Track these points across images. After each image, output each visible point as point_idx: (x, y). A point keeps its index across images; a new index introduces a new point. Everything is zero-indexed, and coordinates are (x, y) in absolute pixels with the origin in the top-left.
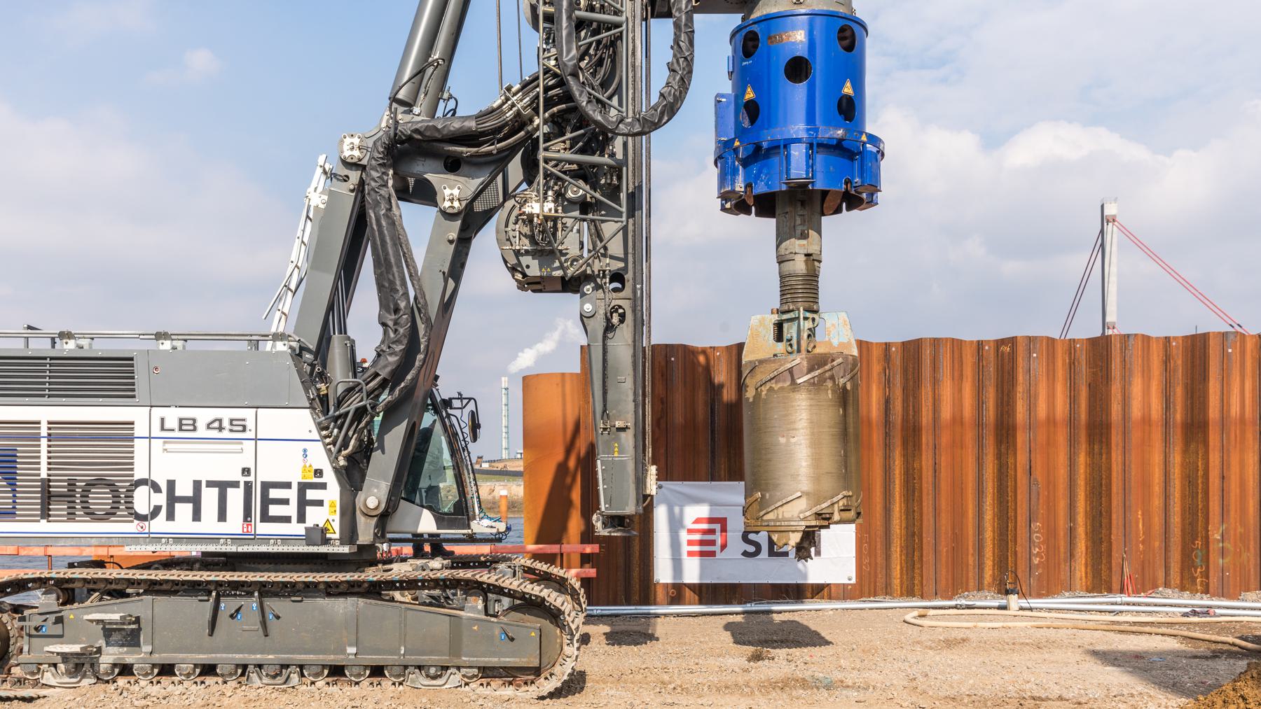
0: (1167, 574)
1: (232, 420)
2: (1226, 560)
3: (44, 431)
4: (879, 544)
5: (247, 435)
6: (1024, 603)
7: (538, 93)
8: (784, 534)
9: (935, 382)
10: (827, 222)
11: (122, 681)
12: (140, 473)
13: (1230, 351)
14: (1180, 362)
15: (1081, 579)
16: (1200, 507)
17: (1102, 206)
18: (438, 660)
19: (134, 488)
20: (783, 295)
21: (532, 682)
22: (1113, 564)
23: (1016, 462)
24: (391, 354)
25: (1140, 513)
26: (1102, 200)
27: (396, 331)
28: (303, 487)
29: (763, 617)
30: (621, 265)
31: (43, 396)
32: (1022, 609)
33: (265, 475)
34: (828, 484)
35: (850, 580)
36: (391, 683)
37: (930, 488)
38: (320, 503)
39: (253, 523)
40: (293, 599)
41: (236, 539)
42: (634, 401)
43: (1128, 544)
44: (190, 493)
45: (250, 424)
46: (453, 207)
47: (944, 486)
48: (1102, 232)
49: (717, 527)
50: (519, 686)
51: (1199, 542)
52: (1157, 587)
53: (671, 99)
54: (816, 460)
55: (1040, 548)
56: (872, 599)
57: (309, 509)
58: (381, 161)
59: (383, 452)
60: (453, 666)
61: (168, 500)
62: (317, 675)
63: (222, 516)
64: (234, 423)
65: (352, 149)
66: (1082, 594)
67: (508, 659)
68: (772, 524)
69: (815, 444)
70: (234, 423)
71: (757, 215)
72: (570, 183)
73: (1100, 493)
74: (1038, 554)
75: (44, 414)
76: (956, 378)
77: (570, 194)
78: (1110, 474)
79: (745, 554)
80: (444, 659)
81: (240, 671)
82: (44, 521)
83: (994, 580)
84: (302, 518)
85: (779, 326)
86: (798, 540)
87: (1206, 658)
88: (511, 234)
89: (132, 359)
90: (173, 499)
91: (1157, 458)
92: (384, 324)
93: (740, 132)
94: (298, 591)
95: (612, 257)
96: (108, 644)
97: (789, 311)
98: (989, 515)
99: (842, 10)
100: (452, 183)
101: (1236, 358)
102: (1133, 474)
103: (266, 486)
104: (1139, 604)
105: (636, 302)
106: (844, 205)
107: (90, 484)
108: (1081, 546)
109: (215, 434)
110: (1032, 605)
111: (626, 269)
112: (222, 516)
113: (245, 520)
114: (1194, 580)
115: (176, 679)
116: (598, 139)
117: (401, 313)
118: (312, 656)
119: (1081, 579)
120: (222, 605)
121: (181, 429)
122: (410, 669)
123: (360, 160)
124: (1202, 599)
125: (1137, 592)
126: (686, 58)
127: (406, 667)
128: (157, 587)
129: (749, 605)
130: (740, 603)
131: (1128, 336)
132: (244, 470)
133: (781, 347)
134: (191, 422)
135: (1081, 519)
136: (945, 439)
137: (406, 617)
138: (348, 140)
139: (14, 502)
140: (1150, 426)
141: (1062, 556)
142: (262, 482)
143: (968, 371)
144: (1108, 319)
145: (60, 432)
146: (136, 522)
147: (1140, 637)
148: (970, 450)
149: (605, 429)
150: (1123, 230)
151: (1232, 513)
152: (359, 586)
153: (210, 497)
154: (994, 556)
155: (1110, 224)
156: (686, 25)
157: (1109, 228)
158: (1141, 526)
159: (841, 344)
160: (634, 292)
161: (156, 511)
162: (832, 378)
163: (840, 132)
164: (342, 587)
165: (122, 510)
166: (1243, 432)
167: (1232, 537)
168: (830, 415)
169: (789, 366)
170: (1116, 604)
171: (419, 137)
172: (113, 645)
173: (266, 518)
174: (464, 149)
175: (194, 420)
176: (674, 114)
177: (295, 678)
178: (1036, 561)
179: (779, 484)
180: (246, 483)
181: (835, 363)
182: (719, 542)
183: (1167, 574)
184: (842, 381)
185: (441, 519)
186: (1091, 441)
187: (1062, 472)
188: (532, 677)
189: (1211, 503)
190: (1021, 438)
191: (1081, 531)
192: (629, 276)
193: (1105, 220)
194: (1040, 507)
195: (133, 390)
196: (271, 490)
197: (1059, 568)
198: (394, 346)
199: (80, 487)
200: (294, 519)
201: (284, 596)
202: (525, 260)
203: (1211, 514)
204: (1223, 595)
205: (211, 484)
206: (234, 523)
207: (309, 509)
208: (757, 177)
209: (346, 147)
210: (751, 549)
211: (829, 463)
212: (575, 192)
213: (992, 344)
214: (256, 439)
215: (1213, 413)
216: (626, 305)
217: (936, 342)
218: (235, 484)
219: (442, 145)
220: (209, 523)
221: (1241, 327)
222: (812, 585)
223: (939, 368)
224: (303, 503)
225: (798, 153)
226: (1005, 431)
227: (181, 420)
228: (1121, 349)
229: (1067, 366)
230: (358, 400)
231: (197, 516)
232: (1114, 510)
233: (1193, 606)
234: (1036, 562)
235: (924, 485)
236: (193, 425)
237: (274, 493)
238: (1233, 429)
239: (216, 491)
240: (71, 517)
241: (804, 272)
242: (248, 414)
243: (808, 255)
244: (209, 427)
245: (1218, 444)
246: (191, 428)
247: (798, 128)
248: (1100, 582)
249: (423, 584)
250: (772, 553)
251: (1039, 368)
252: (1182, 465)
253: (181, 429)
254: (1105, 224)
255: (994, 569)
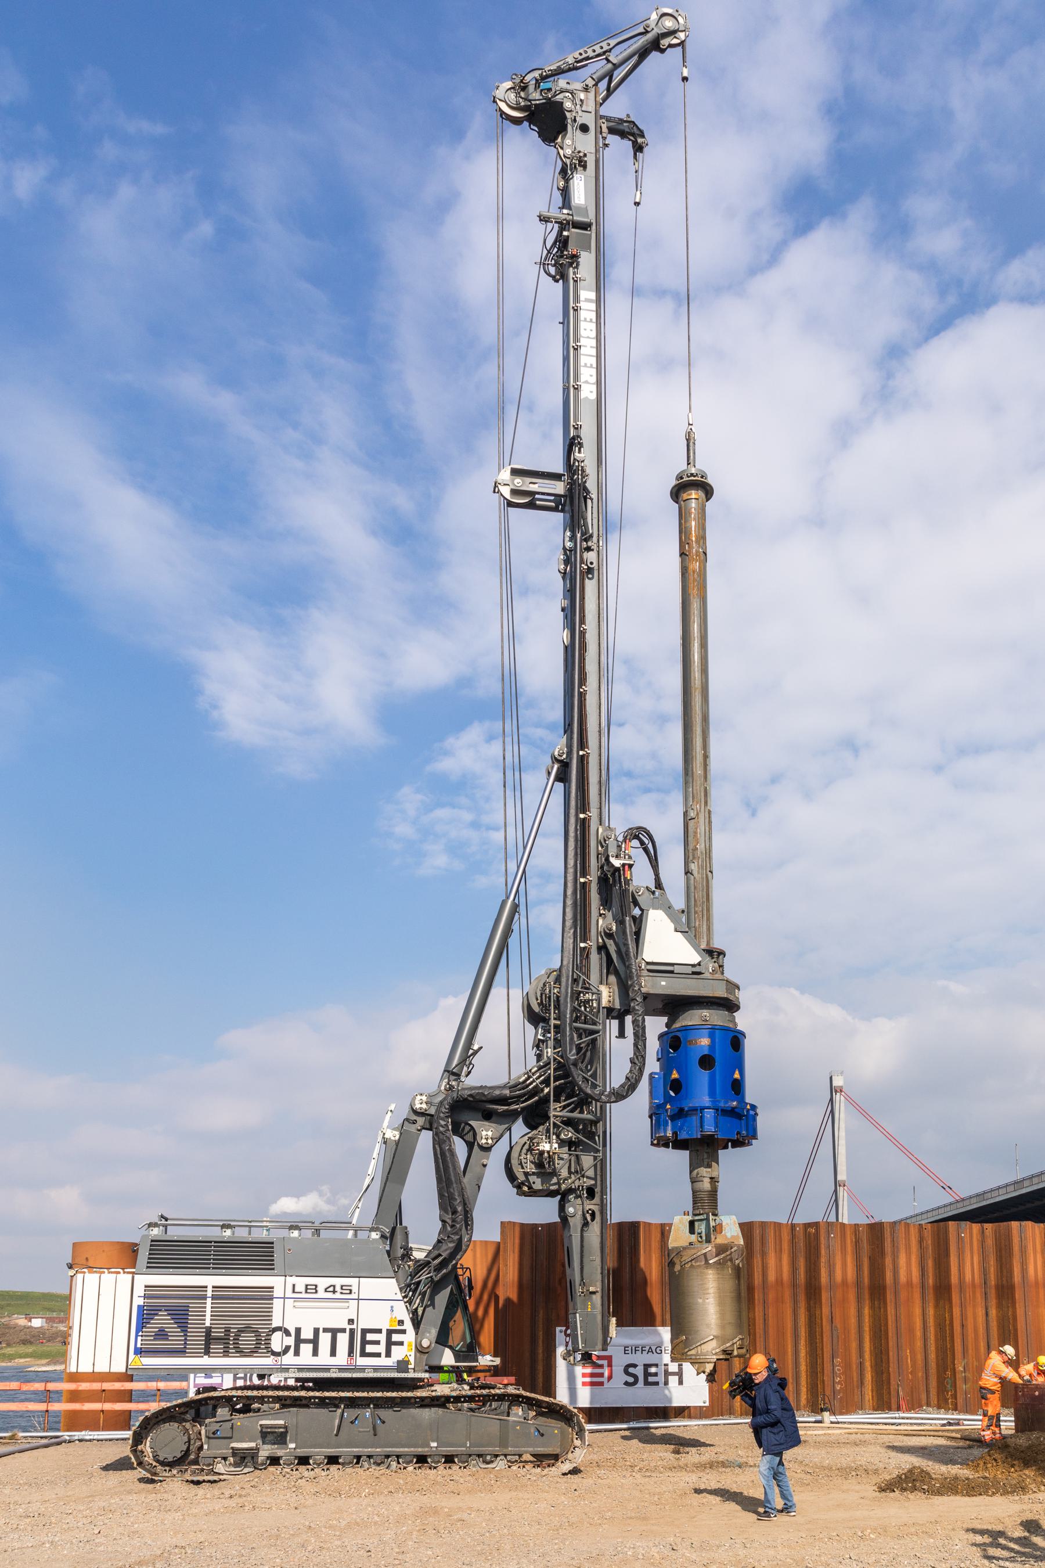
0: (928, 1397)
1: (342, 1286)
2: (968, 1386)
3: (209, 1293)
4: (724, 1375)
5: (354, 1296)
6: (833, 1418)
7: (550, 1074)
8: (702, 1364)
9: (764, 1254)
10: (721, 1153)
11: (271, 1469)
12: (276, 1322)
13: (963, 1235)
14: (930, 1242)
15: (869, 1401)
16: (948, 1347)
17: (831, 1078)
18: (493, 1450)
19: (271, 1333)
20: (696, 1203)
21: (553, 1465)
22: (892, 1390)
23: (822, 1314)
24: (450, 1242)
25: (908, 1351)
26: (830, 1073)
27: (452, 1226)
28: (390, 1333)
29: (646, 1432)
30: (593, 1182)
31: (209, 1268)
32: (832, 1423)
33: (363, 1324)
34: (730, 1330)
35: (704, 1403)
36: (458, 1467)
37: (762, 1333)
38: (401, 1343)
39: (354, 1357)
40: (395, 1409)
41: (341, 1370)
42: (602, 1273)
43: (901, 1374)
44: (311, 1336)
45: (355, 1289)
46: (488, 1143)
47: (772, 1331)
48: (831, 1100)
49: (605, 1362)
50: (545, 1468)
51: (949, 1373)
52: (922, 1406)
53: (633, 1081)
54: (722, 1314)
55: (840, 1378)
56: (721, 1417)
57: (393, 1348)
58: (447, 1115)
59: (434, 1308)
60: (502, 1454)
61: (295, 1341)
62: (409, 1463)
63: (333, 1353)
64: (344, 1288)
65: (421, 1103)
66: (870, 1412)
67: (539, 1449)
68: (694, 1357)
69: (721, 1303)
70: (344, 1288)
71: (673, 1148)
72: (563, 1128)
73: (880, 1337)
74: (839, 1383)
75: (210, 1281)
76: (778, 1250)
77: (562, 1136)
78: (887, 1322)
79: (626, 1383)
80: (497, 1450)
81: (355, 1461)
82: (206, 1357)
83: (808, 1402)
84: (388, 1354)
85: (692, 1224)
86: (711, 1368)
87: (965, 1448)
88: (523, 1161)
89: (272, 1243)
90: (299, 1341)
91: (917, 1311)
92: (443, 1221)
93: (668, 1099)
94: (397, 1404)
95: (588, 1177)
96: (264, 1443)
97: (700, 1214)
98: (803, 1353)
99: (731, 1026)
100: (488, 1127)
101: (967, 1240)
102: (902, 1322)
103: (365, 1332)
104: (911, 1418)
105: (603, 1206)
106: (730, 1144)
107: (241, 1331)
108: (868, 1376)
109: (330, 1295)
110: (839, 1420)
111: (595, 1185)
112: (333, 1353)
113: (349, 1355)
114: (946, 1400)
115: (310, 1467)
116: (584, 1102)
117: (458, 1214)
118: (406, 1449)
119: (869, 1401)
120: (345, 1414)
121: (306, 1292)
122: (474, 1457)
123: (426, 1111)
124: (953, 1414)
125: (909, 1410)
126: (642, 1056)
127: (470, 1455)
128: (298, 1402)
129: (631, 1423)
130: (622, 1422)
131: (895, 1223)
132: (349, 1320)
133: (693, 1238)
134: (314, 1287)
135: (867, 1356)
136: (771, 1296)
137: (470, 1421)
138: (419, 1097)
139: (185, 1343)
140: (912, 1288)
141: (855, 1383)
142: (362, 1329)
143: (786, 1246)
144: (839, 1178)
145: (221, 1294)
146: (272, 1357)
147: (920, 1437)
148: (788, 1305)
149: (582, 1293)
150: (849, 1100)
151: (970, 1351)
152: (437, 1400)
153: (325, 1339)
154: (807, 1385)
155: (838, 1094)
156: (642, 1035)
157: (837, 1097)
158: (909, 1361)
159: (733, 1237)
160: (602, 1200)
161: (287, 1349)
162: (731, 1260)
163: (735, 1103)
164: (426, 1401)
165: (263, 1349)
166: (974, 1293)
167: (971, 1370)
168: (730, 1284)
169: (704, 1251)
170: (895, 1418)
171: (471, 1099)
172: (267, 1444)
173: (364, 1354)
174: (499, 1107)
175: (316, 1286)
176: (634, 1090)
177: (394, 1464)
178: (838, 1387)
179: (698, 1331)
180: (351, 1330)
181: (733, 1250)
182: (606, 1374)
183: (928, 1397)
184: (737, 1262)
185: (458, 1356)
186: (872, 1299)
187: (853, 1321)
188: (553, 1461)
189: (956, 1344)
190: (825, 1296)
191: (868, 1364)
192: (598, 1190)
193: (833, 1090)
194: (840, 1347)
195: (273, 1265)
196: (368, 1334)
197: (853, 1393)
198: (452, 1236)
199: (233, 1332)
200: (383, 1354)
201: (388, 1407)
202: (532, 1179)
203: (956, 1352)
204: (967, 1411)
205: (325, 1330)
206: (342, 1358)
207: (393, 1348)
208: (681, 1128)
209: (417, 1102)
210: (631, 1380)
211: (730, 1317)
212: (565, 1135)
213: (801, 1226)
214: (358, 1299)
215: (954, 1279)
216: (596, 1208)
217: (763, 1225)
218: (343, 1331)
219: (485, 1104)
220: (324, 1358)
221: (951, 1189)
222: (675, 1407)
223: (765, 1243)
224: (390, 1344)
225: (709, 1114)
226: (813, 1291)
227: (307, 1286)
228: (891, 1231)
229: (854, 1243)
230: (426, 1273)
231: (315, 1353)
232: (890, 1349)
233: (947, 1419)
234: (838, 1388)
235: (757, 1330)
236: (315, 1289)
237: (370, 1337)
238: (968, 1290)
239: (329, 1335)
240: (226, 1354)
241: (710, 1189)
242: (353, 1282)
243: (711, 1178)
244: (326, 1291)
245: (958, 1302)
246: (314, 1291)
247: (706, 1100)
248: (883, 1403)
249: (465, 1399)
250: (647, 1383)
251: (836, 1245)
252: (935, 1316)
253: (306, 1292)
254: (834, 1094)
255: (807, 1394)
